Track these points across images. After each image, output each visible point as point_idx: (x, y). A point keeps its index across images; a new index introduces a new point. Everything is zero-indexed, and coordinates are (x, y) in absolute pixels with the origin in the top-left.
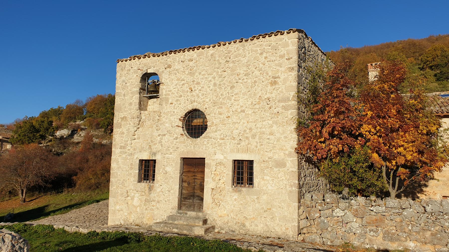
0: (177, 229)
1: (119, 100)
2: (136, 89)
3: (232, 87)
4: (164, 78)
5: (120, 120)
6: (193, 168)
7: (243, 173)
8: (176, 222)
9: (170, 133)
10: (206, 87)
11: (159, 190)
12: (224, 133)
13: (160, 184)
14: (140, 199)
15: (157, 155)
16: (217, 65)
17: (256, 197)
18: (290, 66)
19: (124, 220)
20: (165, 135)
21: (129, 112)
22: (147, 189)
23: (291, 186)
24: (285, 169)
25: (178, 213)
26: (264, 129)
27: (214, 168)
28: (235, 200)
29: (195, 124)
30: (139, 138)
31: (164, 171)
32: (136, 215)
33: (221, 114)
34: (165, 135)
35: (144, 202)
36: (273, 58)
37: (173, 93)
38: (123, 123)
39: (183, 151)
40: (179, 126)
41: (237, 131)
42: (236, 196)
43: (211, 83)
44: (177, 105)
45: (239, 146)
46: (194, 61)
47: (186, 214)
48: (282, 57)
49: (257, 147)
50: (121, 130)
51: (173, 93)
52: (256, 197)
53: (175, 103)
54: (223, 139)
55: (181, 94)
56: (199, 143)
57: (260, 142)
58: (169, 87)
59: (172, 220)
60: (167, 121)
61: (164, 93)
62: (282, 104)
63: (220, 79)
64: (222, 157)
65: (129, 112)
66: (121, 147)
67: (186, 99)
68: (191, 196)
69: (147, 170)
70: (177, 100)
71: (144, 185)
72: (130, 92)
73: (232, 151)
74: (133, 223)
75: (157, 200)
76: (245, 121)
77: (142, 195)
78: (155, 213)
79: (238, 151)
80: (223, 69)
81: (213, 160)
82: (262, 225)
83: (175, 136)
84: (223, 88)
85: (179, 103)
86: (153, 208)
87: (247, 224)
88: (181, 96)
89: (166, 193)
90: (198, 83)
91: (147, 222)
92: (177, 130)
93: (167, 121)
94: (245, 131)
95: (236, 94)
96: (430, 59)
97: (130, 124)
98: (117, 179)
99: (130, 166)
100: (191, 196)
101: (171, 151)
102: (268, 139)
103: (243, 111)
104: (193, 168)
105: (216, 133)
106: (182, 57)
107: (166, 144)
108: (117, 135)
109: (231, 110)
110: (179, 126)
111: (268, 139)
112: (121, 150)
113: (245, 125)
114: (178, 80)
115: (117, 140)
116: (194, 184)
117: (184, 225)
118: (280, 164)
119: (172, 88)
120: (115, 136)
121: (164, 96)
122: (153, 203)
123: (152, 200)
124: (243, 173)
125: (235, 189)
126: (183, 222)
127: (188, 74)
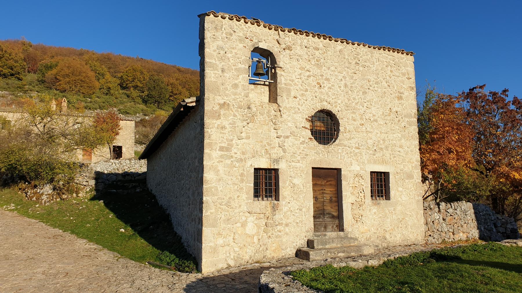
0: (344, 253)
1: (213, 75)
2: (243, 66)
3: (364, 93)
4: (282, 59)
5: (217, 108)
6: (327, 180)
7: (380, 185)
8: (327, 246)
9: (294, 136)
10: (336, 86)
11: (285, 209)
12: (359, 142)
13: (287, 201)
14: (256, 224)
15: (280, 162)
16: (347, 64)
17: (392, 208)
18: (410, 85)
19: (234, 259)
20: (287, 137)
21: (233, 97)
22: (269, 209)
23: (418, 195)
24: (413, 180)
25: (316, 236)
26: (395, 142)
27: (352, 180)
28: (375, 213)
29: (326, 127)
30: (248, 138)
31: (291, 184)
32: (253, 249)
33: (355, 120)
34: (287, 137)
35: (263, 228)
36: (398, 74)
37: (295, 84)
38: (222, 112)
39: (315, 159)
40: (306, 128)
41: (371, 141)
42: (374, 209)
43: (341, 82)
44: (303, 101)
45: (375, 157)
46: (320, 51)
47: (325, 235)
48: (404, 74)
49: (391, 159)
50: (218, 122)
51: (295, 84)
52: (392, 208)
53: (300, 97)
54: (359, 149)
55: (307, 87)
56: (333, 151)
57: (393, 154)
58: (290, 75)
59: (322, 245)
60: (289, 118)
61: (283, 81)
62: (407, 119)
63: (352, 81)
64: (358, 168)
65: (233, 97)
66: (221, 149)
67: (314, 95)
68: (321, 214)
69: (266, 184)
70: (303, 95)
71: (264, 204)
72: (233, 68)
73: (369, 162)
74: (250, 261)
75: (284, 223)
76: (378, 132)
77: (260, 218)
78: (284, 240)
79: (375, 162)
80: (353, 71)
81: (350, 171)
82: (399, 235)
83: (302, 139)
84: (355, 91)
85: (305, 99)
86: (280, 233)
87: (388, 236)
88: (306, 90)
89: (296, 213)
90: (327, 79)
91: (273, 255)
92: (304, 133)
93: (289, 118)
94: (379, 141)
95: (368, 101)
96: (130, 78)
97: (235, 116)
98: (216, 197)
99: (239, 178)
100: (321, 214)
101: (299, 158)
102: (399, 151)
103: (376, 121)
104: (327, 180)
105: (350, 141)
106: (305, 41)
107: (290, 148)
108: (214, 130)
109: (364, 117)
110: (306, 128)
111: (399, 151)
112: (223, 153)
113: (378, 135)
114: (302, 68)
115: (213, 137)
116: (322, 200)
117: (338, 248)
118: (410, 176)
119: (294, 78)
120: (209, 130)
121: (283, 85)
122: (279, 228)
123: (277, 223)
124: (380, 185)
125: (374, 201)
126: (337, 244)
127: (314, 65)
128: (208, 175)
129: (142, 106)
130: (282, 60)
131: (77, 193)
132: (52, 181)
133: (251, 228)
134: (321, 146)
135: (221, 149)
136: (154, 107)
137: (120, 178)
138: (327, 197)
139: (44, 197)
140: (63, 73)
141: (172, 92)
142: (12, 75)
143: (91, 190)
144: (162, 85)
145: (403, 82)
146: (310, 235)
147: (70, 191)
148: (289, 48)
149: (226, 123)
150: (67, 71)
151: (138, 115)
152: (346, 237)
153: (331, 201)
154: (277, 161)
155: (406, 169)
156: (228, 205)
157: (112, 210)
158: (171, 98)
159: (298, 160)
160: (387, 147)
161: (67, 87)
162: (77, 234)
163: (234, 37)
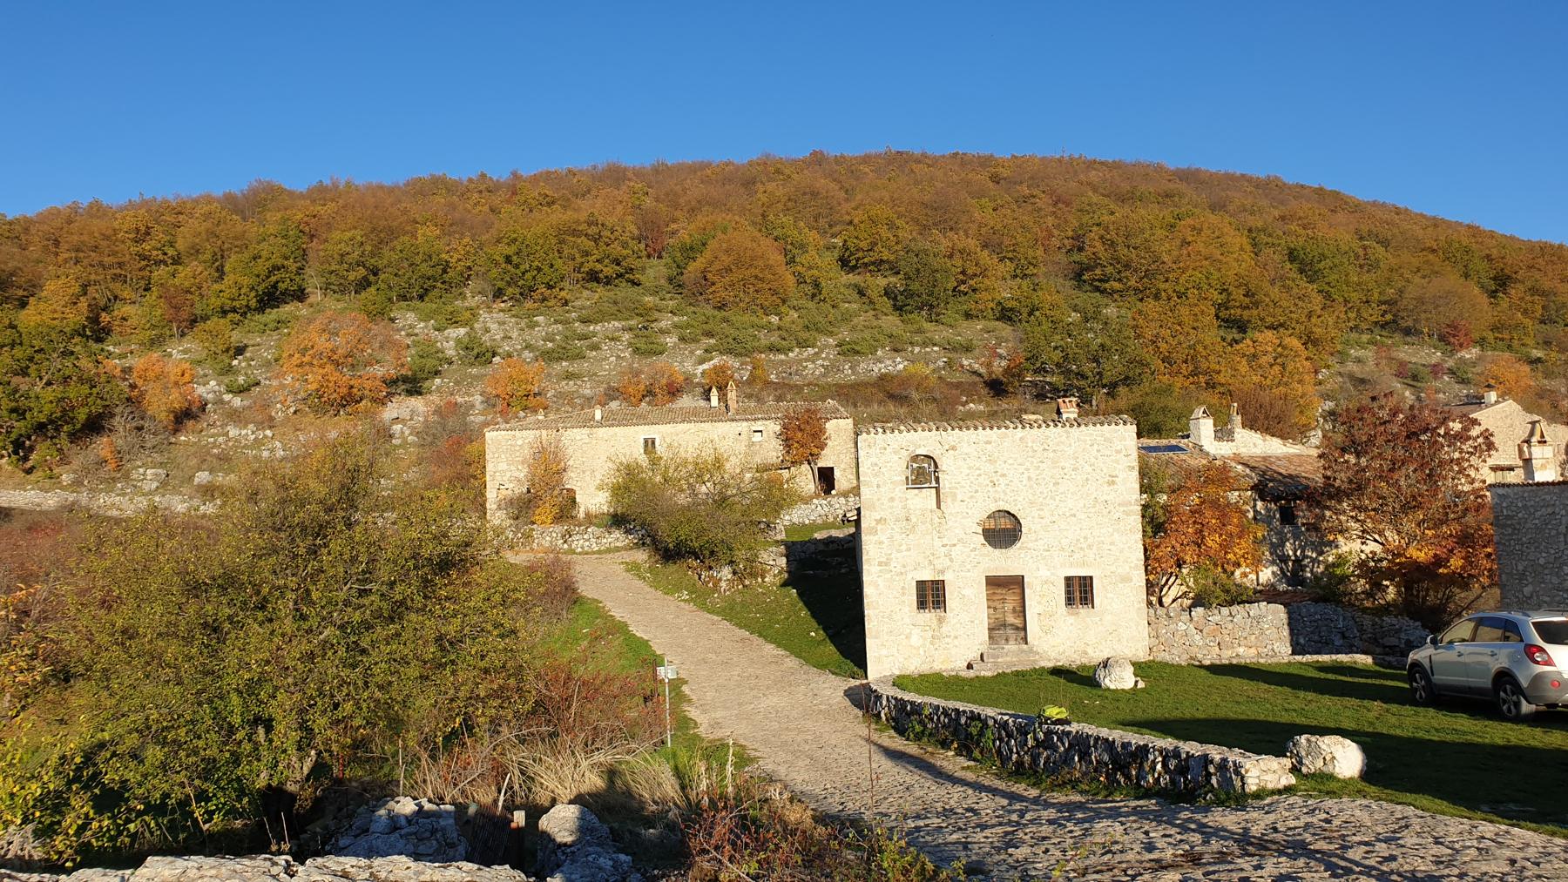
6: (1007, 587)
7: (1080, 591)
29: (1003, 531)
42: (1071, 619)
48: (1118, 452)
66: (880, 564)
69: (931, 595)
71: (929, 616)
79: (1071, 565)
87: (1090, 651)
96: (863, 245)
104: (1007, 587)
118: (1126, 579)
124: (1080, 591)
128: (868, 591)
129: (891, 322)
130: (944, 464)
131: (763, 577)
132: (731, 562)
133: (915, 640)
134: (1019, 545)
135: (880, 564)
136: (920, 319)
137: (821, 547)
138: (1009, 607)
139: (723, 584)
140: (717, 266)
141: (963, 273)
142: (620, 276)
143: (780, 573)
144: (936, 263)
145: (1117, 462)
146: (984, 648)
147: (753, 575)
148: (953, 448)
149: (883, 538)
150: (726, 260)
151: (879, 353)
152: (1031, 651)
153: (1014, 610)
154: (942, 572)
155: (1120, 570)
156: (890, 617)
157: (807, 604)
158: (962, 288)
159: (969, 568)
160: (1090, 547)
161: (728, 295)
162: (765, 638)
163: (889, 450)
